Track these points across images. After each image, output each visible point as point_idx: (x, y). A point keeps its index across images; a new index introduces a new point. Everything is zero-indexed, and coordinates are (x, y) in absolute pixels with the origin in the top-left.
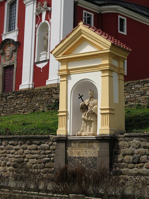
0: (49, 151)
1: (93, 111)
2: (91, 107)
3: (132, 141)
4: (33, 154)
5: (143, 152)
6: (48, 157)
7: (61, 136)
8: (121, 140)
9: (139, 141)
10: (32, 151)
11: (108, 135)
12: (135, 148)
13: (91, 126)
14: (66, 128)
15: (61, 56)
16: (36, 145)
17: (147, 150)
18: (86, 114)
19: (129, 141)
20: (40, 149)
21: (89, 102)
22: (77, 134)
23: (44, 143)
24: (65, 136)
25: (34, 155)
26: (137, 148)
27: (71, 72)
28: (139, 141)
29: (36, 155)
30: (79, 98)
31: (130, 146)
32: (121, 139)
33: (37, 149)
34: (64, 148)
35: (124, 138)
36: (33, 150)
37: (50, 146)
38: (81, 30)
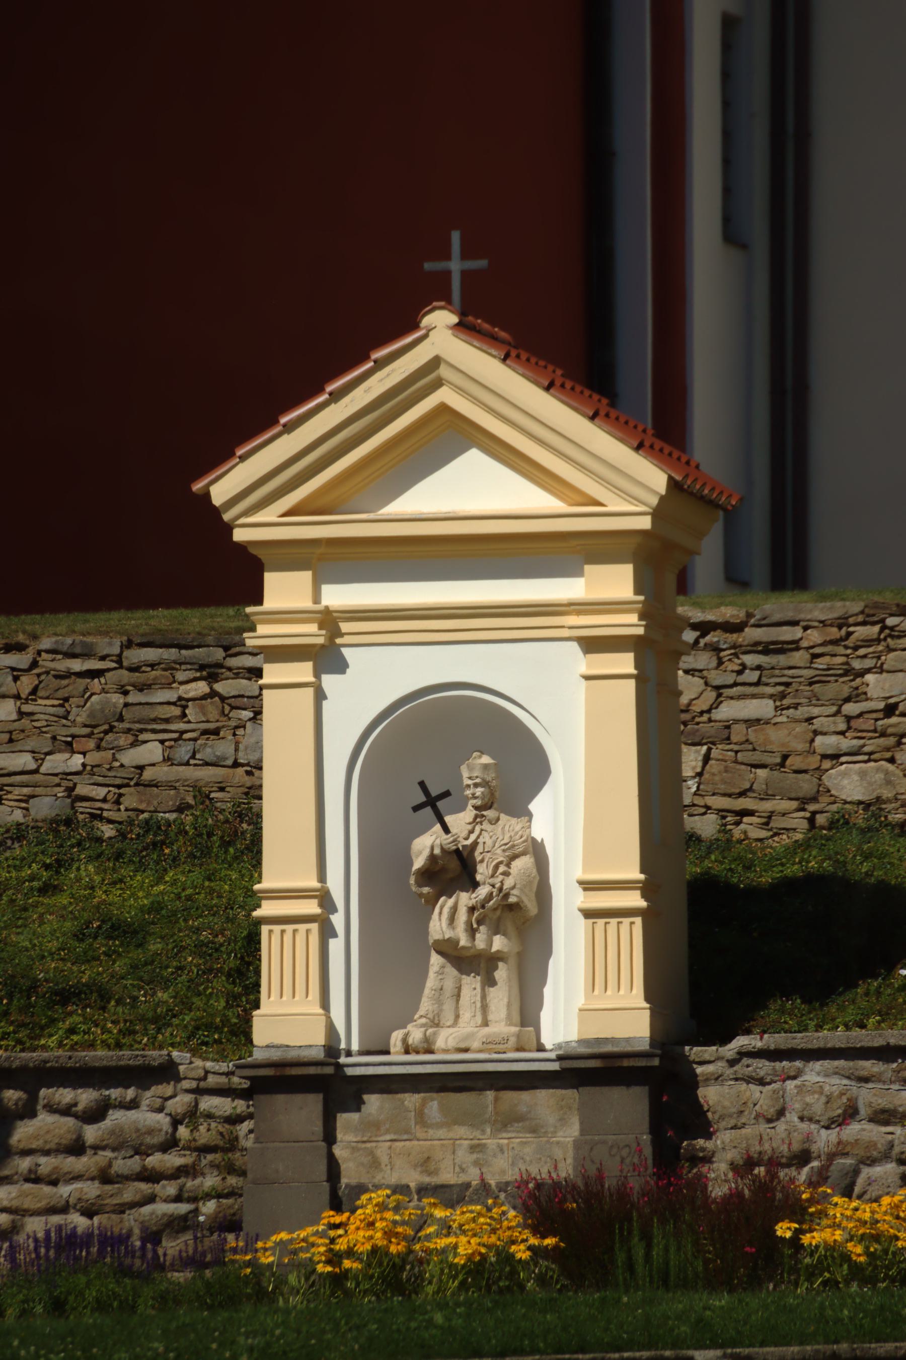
0: (174, 1160)
1: (514, 892)
2: (496, 867)
3: (794, 1078)
4: (54, 1183)
5: (872, 1145)
6: (178, 1199)
7: (292, 1055)
8: (718, 1078)
9: (848, 1078)
10: (43, 1160)
11: (645, 1046)
12: (818, 1122)
13: (490, 982)
14: (325, 1003)
15: (274, 519)
16: (70, 1121)
17: (898, 1130)
18: (454, 909)
19: (769, 1084)
20: (104, 1148)
21: (471, 832)
22: (404, 1041)
23: (133, 1105)
24: (320, 1055)
25: (65, 1190)
26: (833, 1123)
27: (345, 627)
28: (845, 1082)
29: (78, 1185)
30: (416, 809)
31: (781, 1113)
32: (710, 1068)
33: (77, 1148)
34: (318, 1127)
35: (732, 1063)
36: (47, 1153)
37: (176, 1122)
38: (436, 362)
